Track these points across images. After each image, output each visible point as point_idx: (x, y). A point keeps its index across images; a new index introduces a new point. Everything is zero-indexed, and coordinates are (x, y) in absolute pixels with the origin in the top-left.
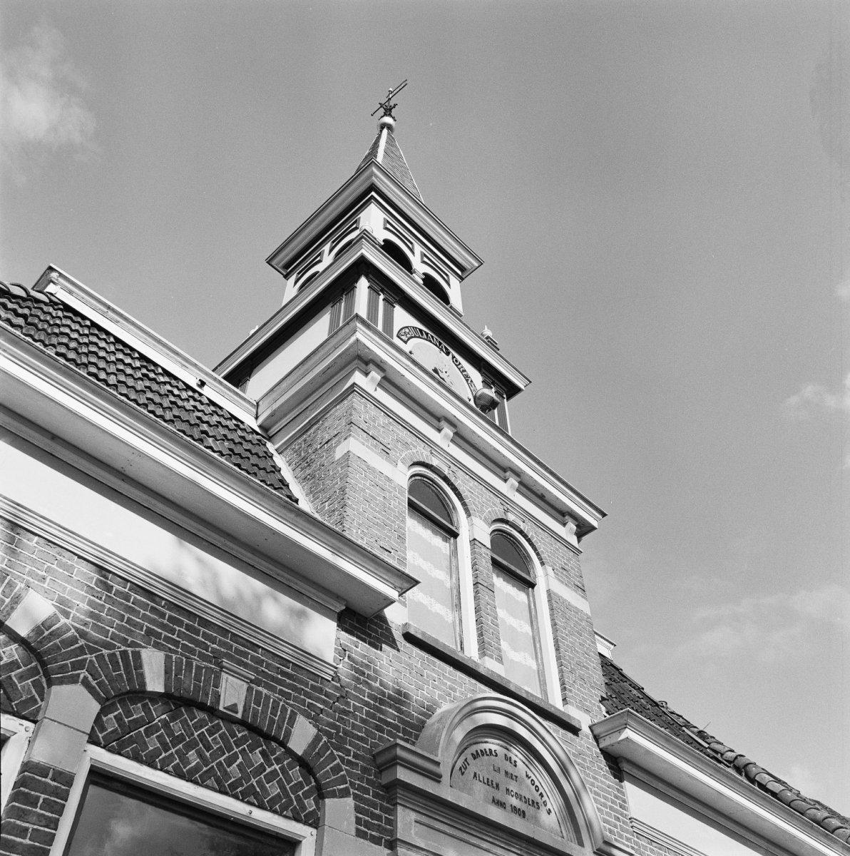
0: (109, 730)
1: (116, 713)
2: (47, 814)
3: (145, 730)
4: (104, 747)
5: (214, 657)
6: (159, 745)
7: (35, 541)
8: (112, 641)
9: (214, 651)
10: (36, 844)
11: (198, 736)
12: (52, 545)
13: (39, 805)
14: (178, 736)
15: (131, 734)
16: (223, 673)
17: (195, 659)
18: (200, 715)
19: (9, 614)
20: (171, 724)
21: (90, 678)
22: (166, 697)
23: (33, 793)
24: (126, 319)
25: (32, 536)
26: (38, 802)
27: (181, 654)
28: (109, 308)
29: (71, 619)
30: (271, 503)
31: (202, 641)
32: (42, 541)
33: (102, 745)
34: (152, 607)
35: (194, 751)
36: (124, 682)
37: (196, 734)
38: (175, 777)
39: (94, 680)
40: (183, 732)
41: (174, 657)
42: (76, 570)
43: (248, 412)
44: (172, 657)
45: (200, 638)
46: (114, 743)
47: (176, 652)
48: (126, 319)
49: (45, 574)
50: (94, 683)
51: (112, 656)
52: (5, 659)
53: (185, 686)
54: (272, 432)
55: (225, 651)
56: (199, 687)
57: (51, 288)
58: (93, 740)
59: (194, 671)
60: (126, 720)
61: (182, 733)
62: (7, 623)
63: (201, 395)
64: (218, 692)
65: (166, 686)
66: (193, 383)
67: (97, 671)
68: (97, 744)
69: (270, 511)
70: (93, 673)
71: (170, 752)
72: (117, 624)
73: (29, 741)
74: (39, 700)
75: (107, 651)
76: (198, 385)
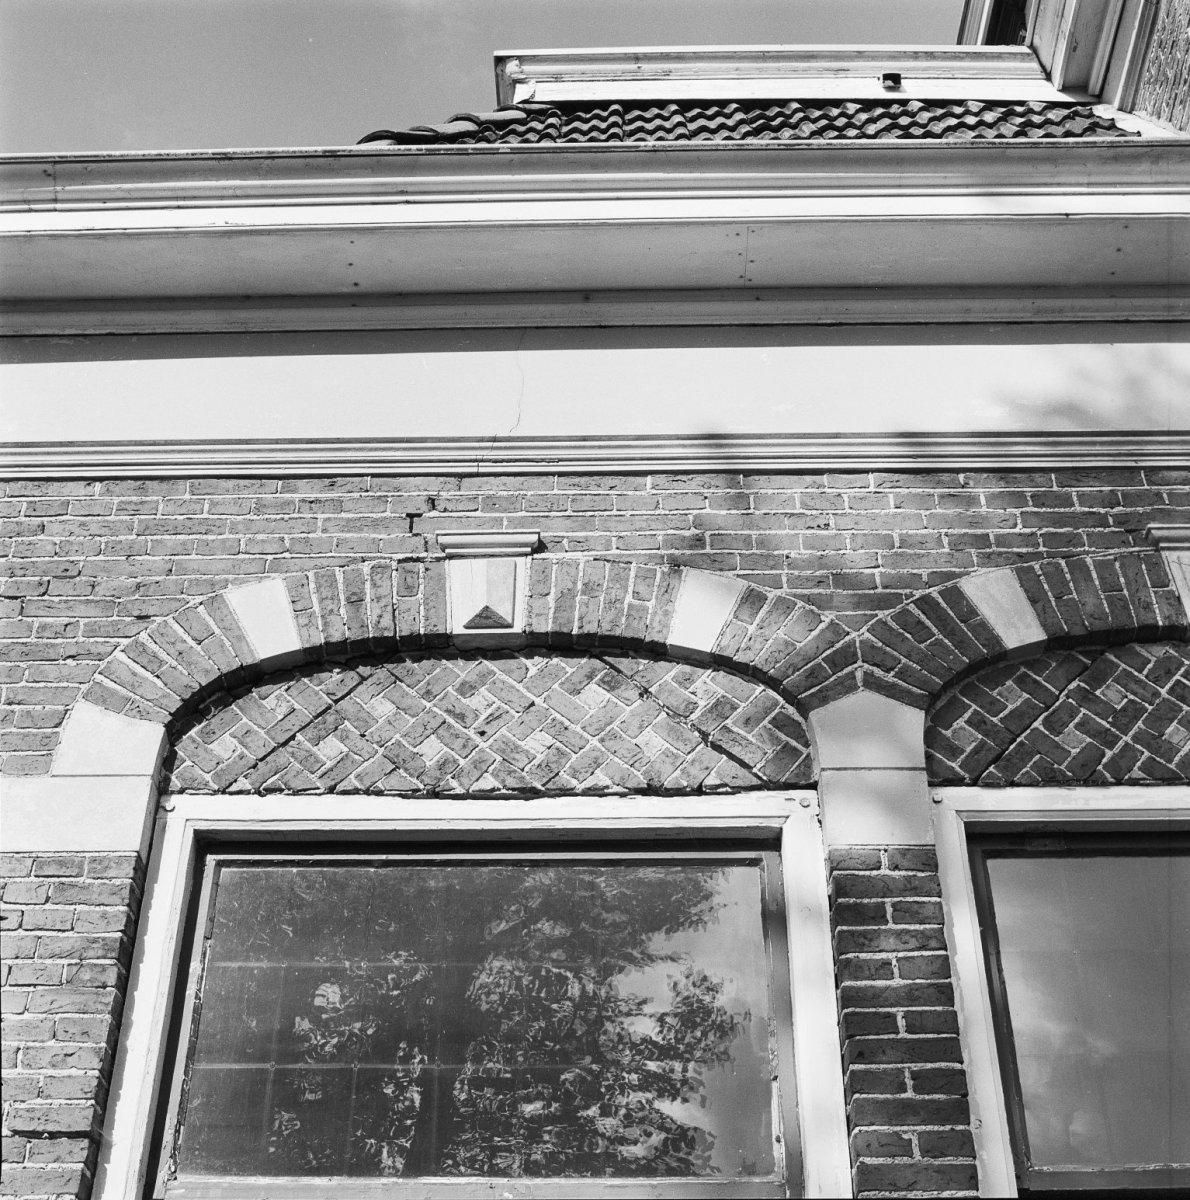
0: (968, 750)
1: (967, 716)
2: (912, 927)
3: (1045, 723)
4: (974, 783)
5: (1129, 531)
6: (1089, 740)
7: (649, 486)
8: (888, 591)
9: (1120, 520)
10: (918, 981)
11: (1171, 691)
12: (684, 478)
13: (889, 916)
14: (1124, 709)
15: (1019, 740)
16: (1164, 554)
17: (1087, 553)
18: (1155, 653)
19: (667, 626)
20: (1098, 693)
21: (878, 672)
22: (1058, 645)
23: (866, 901)
24: (679, 57)
25: (639, 480)
26: (885, 912)
27: (1050, 555)
28: (636, 58)
29: (785, 586)
30: (1081, 168)
31: (1084, 513)
32: (661, 479)
33: (967, 781)
34: (942, 497)
35: (1175, 723)
36: (950, 652)
37: (1163, 692)
38: (1159, 785)
39: (888, 671)
40: (1132, 697)
41: (1037, 567)
42: (751, 499)
43: (1025, 76)
44: (1032, 568)
45: (1078, 508)
46: (991, 769)
47: (1038, 556)
48: (679, 57)
49: (697, 532)
50: (890, 677)
51: (903, 617)
52: (702, 703)
53: (1089, 608)
54: (1095, 84)
55: (1149, 509)
56: (1122, 599)
57: (521, 93)
58: (939, 777)
59: (1094, 575)
60: (995, 719)
61: (1132, 701)
62: (669, 642)
63: (904, 102)
64: (1171, 592)
65: (1044, 626)
66: (876, 90)
67: (885, 653)
68: (955, 781)
69: (1089, 185)
70: (878, 660)
71: (1121, 743)
72: (883, 556)
73: (820, 822)
74: (800, 747)
75: (887, 612)
76: (889, 89)
